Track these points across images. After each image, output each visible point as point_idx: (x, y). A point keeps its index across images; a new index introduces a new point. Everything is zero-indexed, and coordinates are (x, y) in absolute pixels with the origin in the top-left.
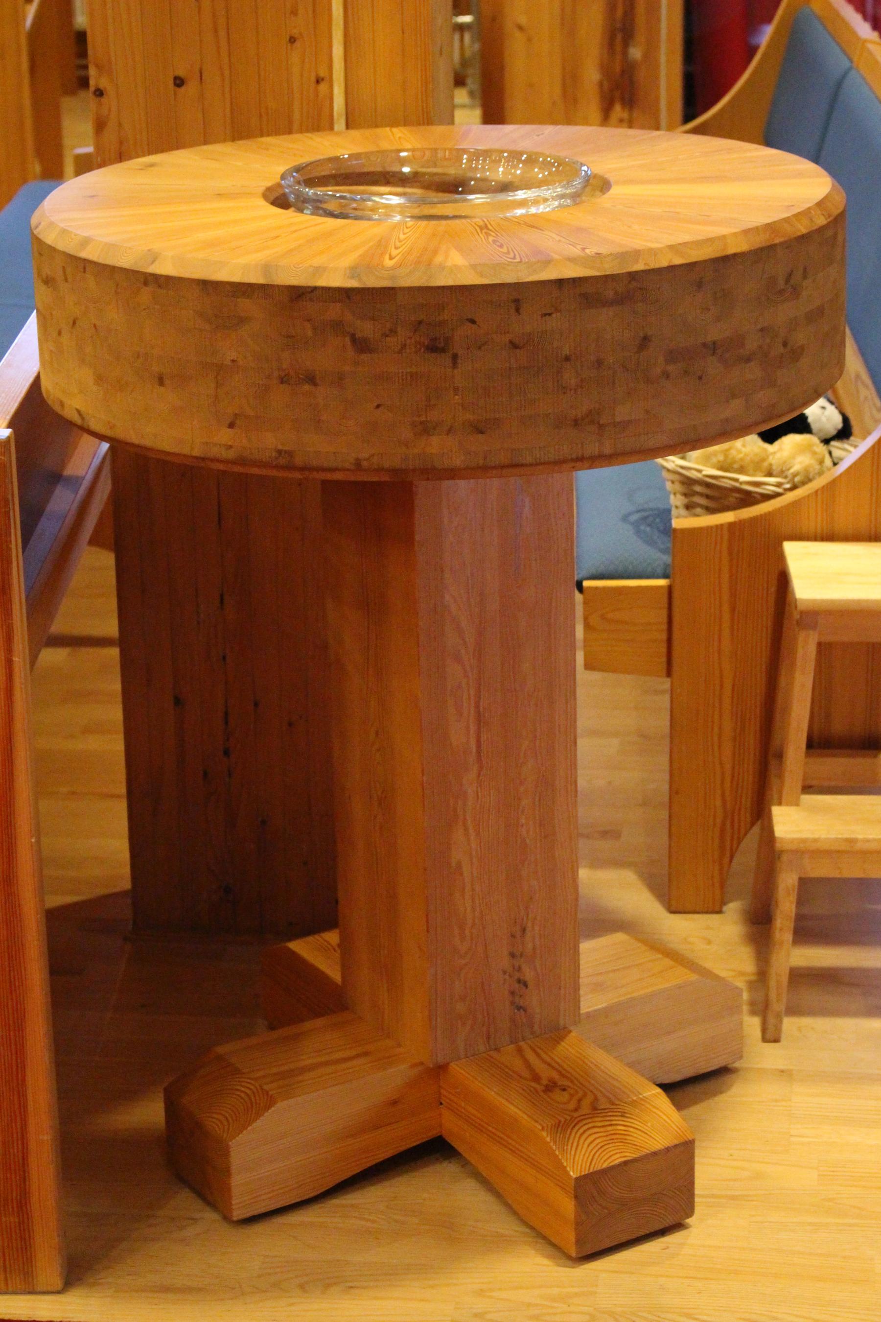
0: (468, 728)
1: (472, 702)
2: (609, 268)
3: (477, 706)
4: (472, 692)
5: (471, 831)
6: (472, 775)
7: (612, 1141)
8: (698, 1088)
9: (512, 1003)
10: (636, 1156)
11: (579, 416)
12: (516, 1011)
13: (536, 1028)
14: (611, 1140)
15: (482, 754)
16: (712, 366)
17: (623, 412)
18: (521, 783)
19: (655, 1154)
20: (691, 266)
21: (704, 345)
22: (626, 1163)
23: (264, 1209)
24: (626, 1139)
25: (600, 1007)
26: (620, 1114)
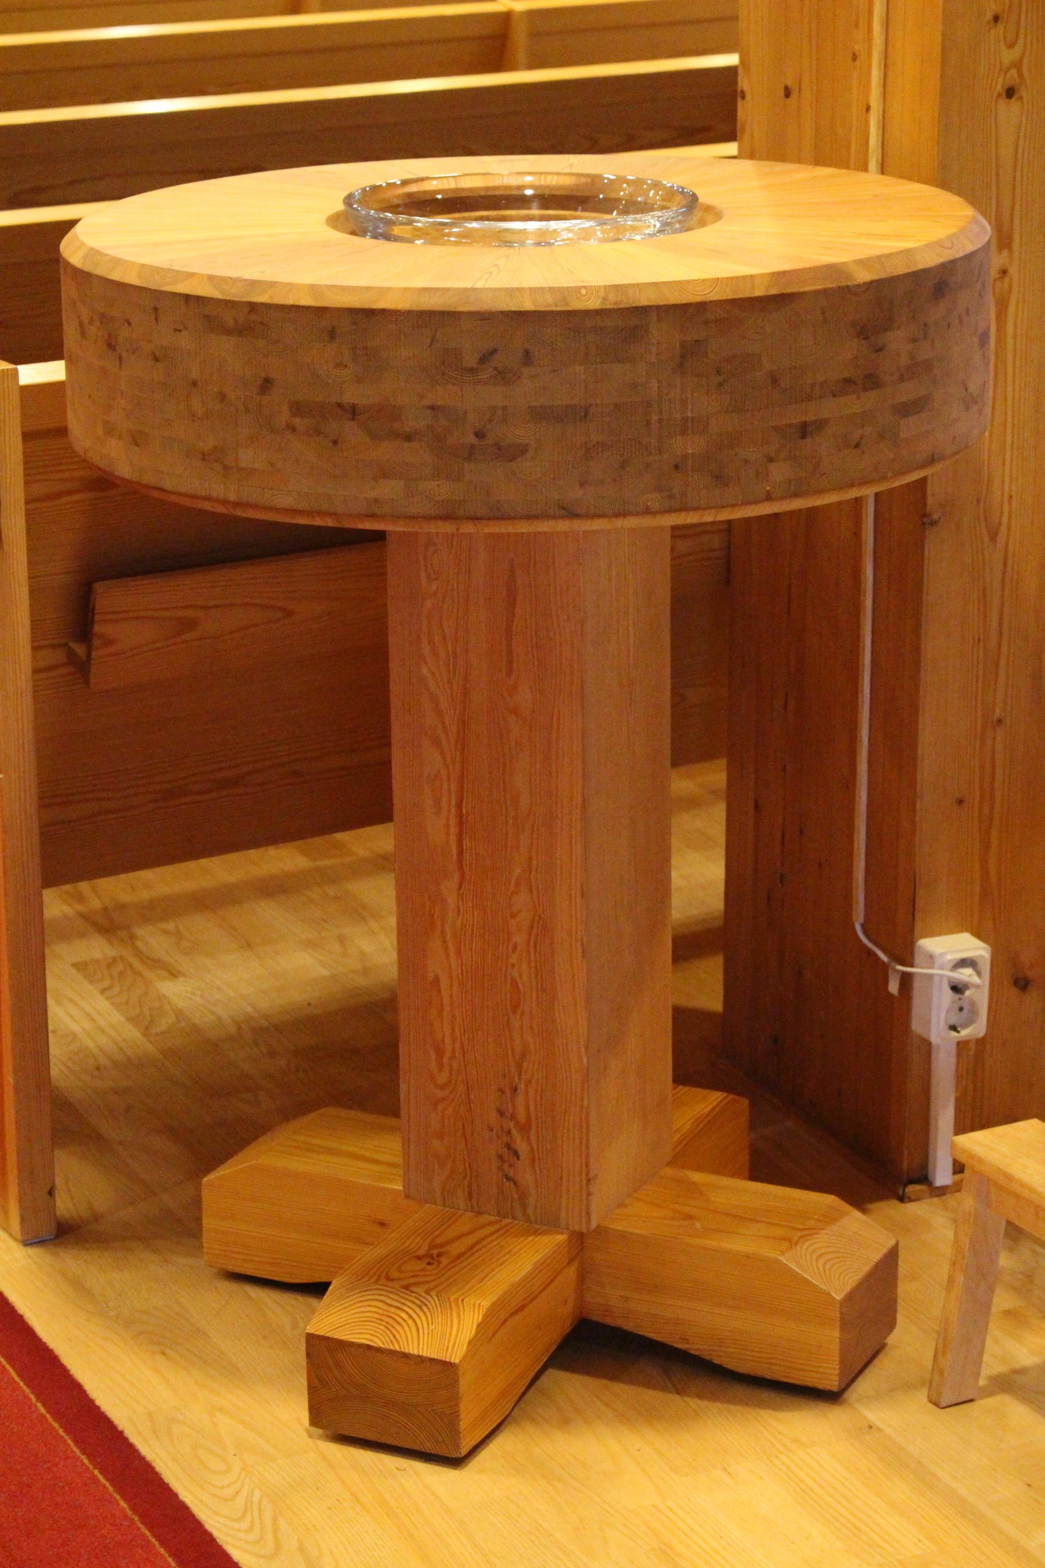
0: (447, 826)
1: (453, 803)
2: (234, 294)
3: (459, 806)
4: (453, 788)
5: (450, 945)
6: (453, 883)
7: (379, 1321)
8: (765, 1395)
9: (500, 1169)
10: (382, 1346)
11: (206, 449)
12: (505, 1180)
13: (530, 1211)
14: (379, 1320)
15: (464, 864)
16: (352, 433)
17: (247, 457)
18: (513, 916)
19: (405, 1356)
20: (321, 311)
21: (340, 405)
22: (369, 1347)
23: (252, 1271)
24: (394, 1327)
25: (639, 1232)
26: (419, 1303)
